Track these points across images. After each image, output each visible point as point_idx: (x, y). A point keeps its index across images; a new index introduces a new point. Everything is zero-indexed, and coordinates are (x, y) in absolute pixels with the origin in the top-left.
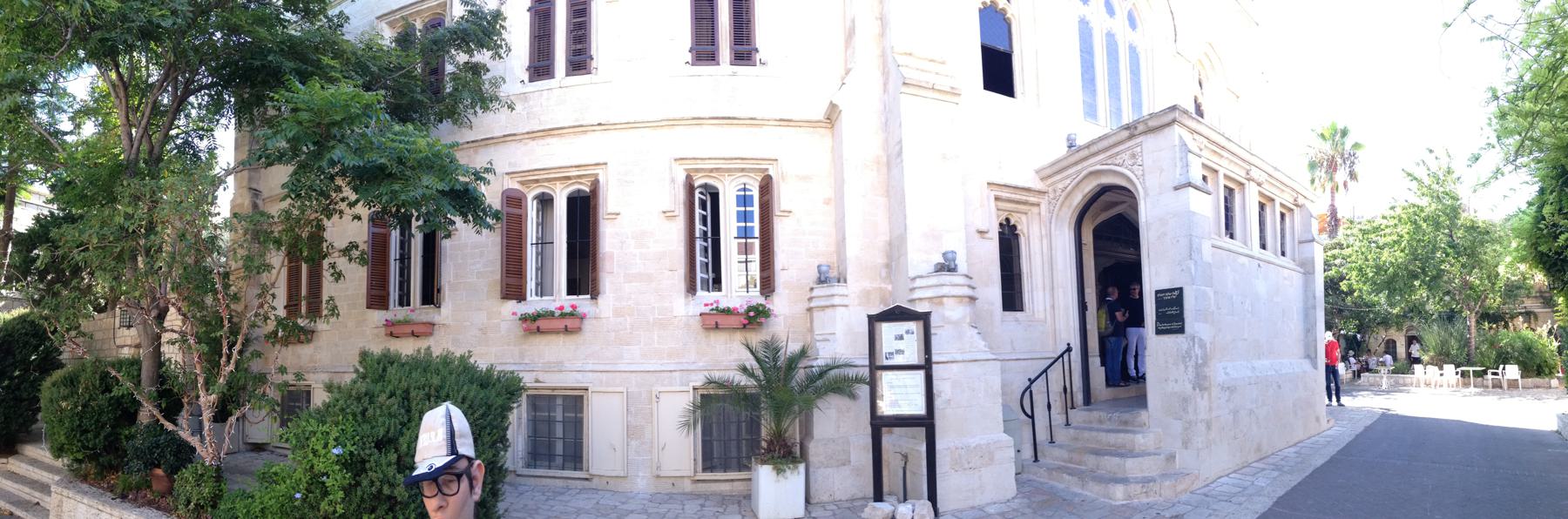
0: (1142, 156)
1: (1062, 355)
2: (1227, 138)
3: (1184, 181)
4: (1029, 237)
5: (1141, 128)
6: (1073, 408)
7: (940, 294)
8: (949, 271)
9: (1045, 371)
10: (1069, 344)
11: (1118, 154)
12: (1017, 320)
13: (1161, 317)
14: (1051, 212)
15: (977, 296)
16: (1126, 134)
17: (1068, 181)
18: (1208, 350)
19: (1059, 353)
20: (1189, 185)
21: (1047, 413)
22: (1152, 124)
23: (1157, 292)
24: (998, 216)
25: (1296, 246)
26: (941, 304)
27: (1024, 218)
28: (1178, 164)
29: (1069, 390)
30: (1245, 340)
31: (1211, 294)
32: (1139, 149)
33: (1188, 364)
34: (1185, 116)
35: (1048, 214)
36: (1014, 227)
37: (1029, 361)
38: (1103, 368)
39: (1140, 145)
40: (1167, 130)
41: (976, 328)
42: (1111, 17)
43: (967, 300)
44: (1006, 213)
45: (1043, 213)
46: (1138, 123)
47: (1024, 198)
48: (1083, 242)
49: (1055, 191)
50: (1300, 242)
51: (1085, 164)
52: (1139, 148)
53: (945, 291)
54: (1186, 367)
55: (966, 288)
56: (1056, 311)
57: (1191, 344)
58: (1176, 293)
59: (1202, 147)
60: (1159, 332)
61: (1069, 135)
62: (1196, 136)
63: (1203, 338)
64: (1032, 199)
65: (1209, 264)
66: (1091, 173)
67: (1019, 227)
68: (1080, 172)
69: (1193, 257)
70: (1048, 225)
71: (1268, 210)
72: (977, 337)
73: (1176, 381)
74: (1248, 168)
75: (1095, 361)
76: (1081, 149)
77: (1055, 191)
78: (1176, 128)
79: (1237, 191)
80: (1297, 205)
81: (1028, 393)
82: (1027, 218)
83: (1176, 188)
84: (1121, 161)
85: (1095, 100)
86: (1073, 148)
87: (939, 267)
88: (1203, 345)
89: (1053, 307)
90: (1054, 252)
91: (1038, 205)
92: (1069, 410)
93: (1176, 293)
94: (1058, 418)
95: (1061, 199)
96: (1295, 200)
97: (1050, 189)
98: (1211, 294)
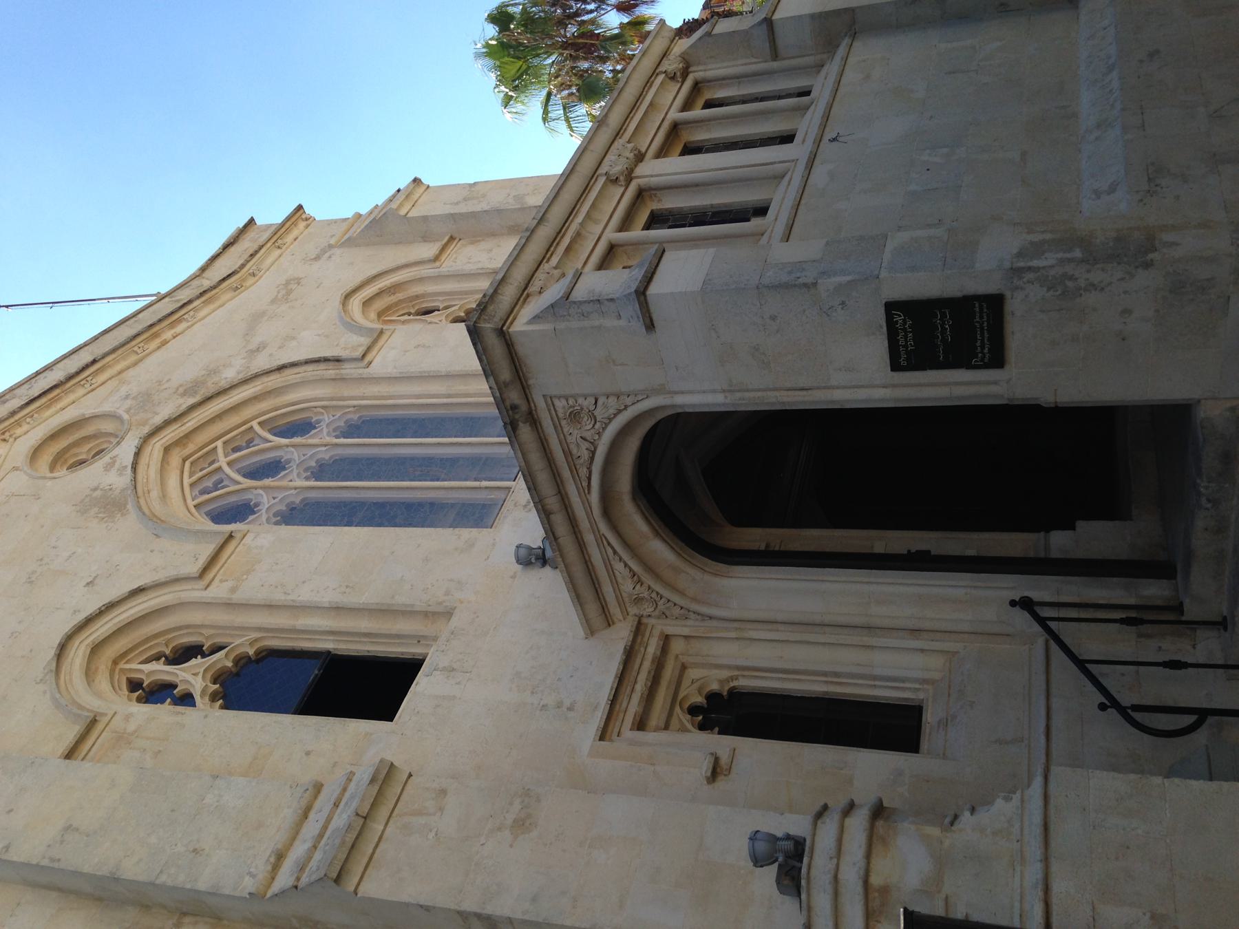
0: (575, 397)
1: (1042, 622)
2: (539, 223)
3: (633, 308)
4: (738, 668)
5: (514, 396)
6: (1179, 608)
7: (859, 889)
8: (799, 857)
9: (1081, 664)
10: (1013, 603)
11: (568, 453)
12: (944, 724)
13: (960, 357)
14: (686, 614)
15: (871, 799)
16: (525, 431)
17: (619, 566)
18: (1048, 236)
19: (1037, 628)
20: (641, 294)
21: (1190, 670)
22: (506, 374)
23: (895, 366)
24: (683, 729)
25: (786, 63)
26: (885, 890)
27: (692, 674)
28: (597, 323)
29: (1133, 614)
30: (1024, 154)
31: (904, 236)
32: (560, 404)
33: (1082, 283)
34: (491, 308)
35: (689, 622)
36: (712, 697)
37: (1056, 703)
38: (1081, 525)
39: (550, 400)
40: (522, 349)
41: (956, 817)
42: (284, 468)
43: (880, 823)
44: (677, 709)
45: (686, 631)
46: (503, 401)
47: (647, 665)
48: (763, 548)
49: (638, 600)
50: (775, 55)
51: (584, 524)
52: (557, 402)
53: (851, 876)
54: (1092, 286)
55: (848, 821)
56: (927, 625)
57: (1031, 276)
58: (899, 319)
59: (557, 273)
60: (997, 360)
61: (519, 561)
62: (533, 288)
63: (1015, 251)
64: (652, 648)
65: (827, 243)
66: (606, 512)
67: (715, 687)
68: (600, 539)
69: (810, 280)
70: (714, 623)
71: (700, 136)
72: (983, 816)
73: (1127, 312)
74: (602, 180)
75: (1060, 542)
76: (551, 534)
77: (638, 600)
78: (520, 325)
79: (655, 205)
80: (685, 73)
81: (1138, 716)
82: (696, 665)
83: (650, 326)
84: (584, 445)
85: (453, 505)
86: (549, 554)
87: (786, 882)
88: (1038, 249)
89: (915, 632)
90: (780, 617)
91: (666, 639)
92: (1184, 618)
93: (899, 319)
94: (1207, 646)
95: (658, 587)
96: (673, 78)
97: (633, 610)
98: (904, 236)
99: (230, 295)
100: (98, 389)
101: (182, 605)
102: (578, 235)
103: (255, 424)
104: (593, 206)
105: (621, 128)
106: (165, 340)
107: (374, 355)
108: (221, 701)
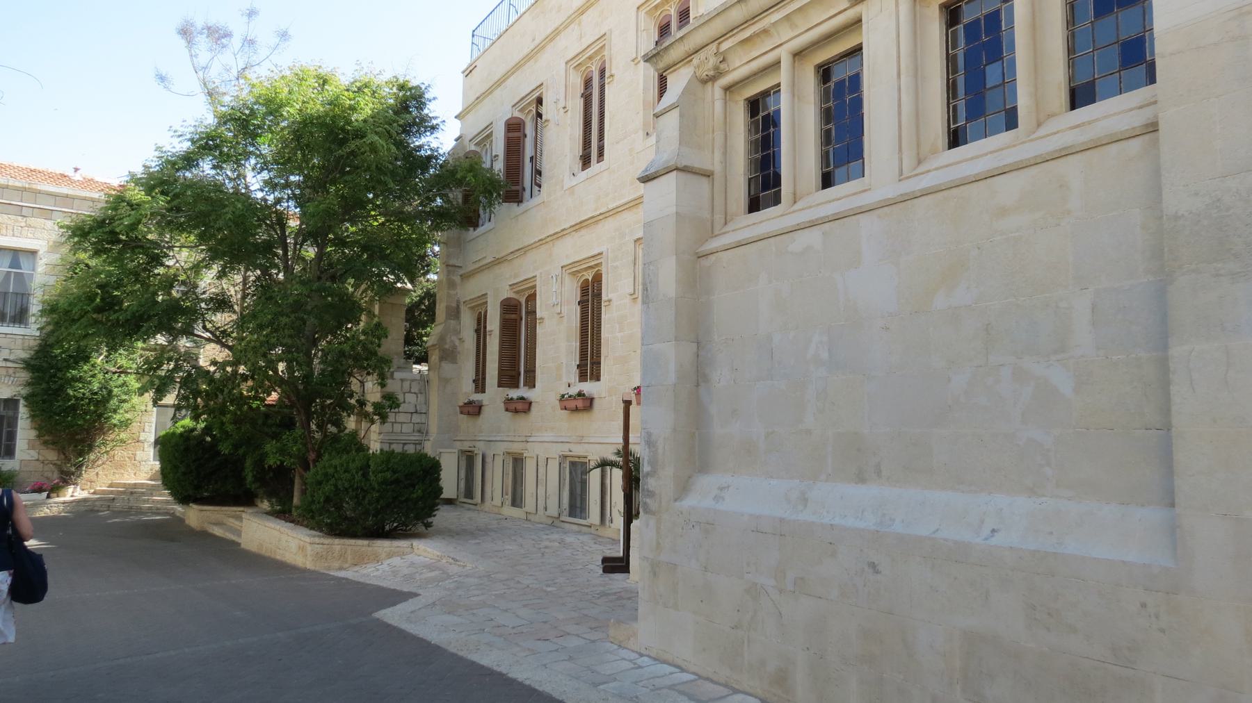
102: (765, 31)
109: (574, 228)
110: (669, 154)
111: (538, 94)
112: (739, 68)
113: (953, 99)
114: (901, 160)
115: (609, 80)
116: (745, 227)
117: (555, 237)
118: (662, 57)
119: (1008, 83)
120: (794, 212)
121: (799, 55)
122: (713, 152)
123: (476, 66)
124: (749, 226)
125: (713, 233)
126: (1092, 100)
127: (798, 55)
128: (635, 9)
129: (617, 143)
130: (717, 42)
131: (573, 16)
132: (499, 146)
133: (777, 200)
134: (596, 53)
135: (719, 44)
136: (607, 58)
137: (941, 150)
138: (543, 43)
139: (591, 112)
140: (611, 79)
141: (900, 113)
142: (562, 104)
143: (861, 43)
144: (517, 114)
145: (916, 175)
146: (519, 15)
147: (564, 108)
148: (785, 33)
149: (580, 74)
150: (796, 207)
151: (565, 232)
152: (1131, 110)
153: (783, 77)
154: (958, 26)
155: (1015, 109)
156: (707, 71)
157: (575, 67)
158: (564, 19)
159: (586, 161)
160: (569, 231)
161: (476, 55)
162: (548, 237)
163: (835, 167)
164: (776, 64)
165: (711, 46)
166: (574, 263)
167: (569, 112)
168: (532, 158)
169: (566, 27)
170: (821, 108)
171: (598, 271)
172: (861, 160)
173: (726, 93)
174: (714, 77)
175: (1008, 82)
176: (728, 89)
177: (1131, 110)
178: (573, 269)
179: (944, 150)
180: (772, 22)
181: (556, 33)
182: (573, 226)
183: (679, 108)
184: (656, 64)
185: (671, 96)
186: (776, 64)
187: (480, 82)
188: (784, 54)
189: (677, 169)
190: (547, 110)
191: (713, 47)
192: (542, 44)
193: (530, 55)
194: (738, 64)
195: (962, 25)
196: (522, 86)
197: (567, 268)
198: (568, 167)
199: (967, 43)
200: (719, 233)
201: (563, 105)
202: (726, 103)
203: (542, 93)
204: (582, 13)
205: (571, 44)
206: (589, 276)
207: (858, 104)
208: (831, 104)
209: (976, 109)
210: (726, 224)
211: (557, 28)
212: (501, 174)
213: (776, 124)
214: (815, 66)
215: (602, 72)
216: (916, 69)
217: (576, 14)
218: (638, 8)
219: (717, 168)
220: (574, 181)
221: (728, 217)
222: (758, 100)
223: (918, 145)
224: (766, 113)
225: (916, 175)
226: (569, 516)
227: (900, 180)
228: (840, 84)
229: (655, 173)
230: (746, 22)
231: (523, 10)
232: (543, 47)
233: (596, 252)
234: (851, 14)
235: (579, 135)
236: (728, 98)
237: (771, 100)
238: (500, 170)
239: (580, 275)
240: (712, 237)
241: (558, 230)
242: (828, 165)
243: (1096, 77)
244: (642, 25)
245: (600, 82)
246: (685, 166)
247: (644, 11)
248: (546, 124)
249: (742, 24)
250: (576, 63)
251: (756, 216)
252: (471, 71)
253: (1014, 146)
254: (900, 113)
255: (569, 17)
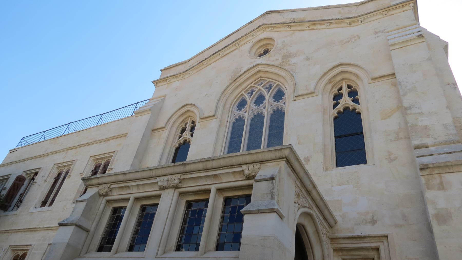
99: (345, 25)
100: (288, 31)
101: (350, 73)
102: (128, 187)
103: (243, 92)
104: (143, 185)
105: (209, 169)
106: (314, 28)
107: (300, 99)
108: (352, 98)
109: (25, 230)
110: (76, 217)
111: (37, 171)
112: (115, 195)
113: (182, 233)
114: (158, 250)
115: (68, 177)
116: (94, 257)
117: (14, 231)
118: (89, 181)
119: (199, 234)
120: (114, 257)
121: (137, 199)
122: (93, 223)
123: (17, 151)
124: (95, 257)
125: (80, 255)
126: (222, 250)
127: (137, 199)
128: (89, 156)
129: (61, 201)
130: (111, 184)
131: (66, 149)
132: (9, 185)
133: (109, 250)
134: (68, 165)
135: (111, 185)
136: (71, 169)
137: (173, 250)
138: (49, 154)
139: (56, 186)
140: (69, 177)
141: (163, 233)
142: (45, 178)
143: (159, 203)
144: (24, 175)
145: (162, 258)
146: (45, 140)
147: (45, 180)
148: (135, 190)
149: (58, 170)
150: (116, 255)
151: (19, 231)
152: (232, 257)
153: (129, 204)
154: (190, 210)
155: (199, 244)
156: (103, 192)
157: (57, 167)
158: (61, 149)
159: (44, 204)
160: (21, 230)
161: (19, 146)
162: (11, 230)
163: (136, 244)
164: (128, 199)
165: (108, 184)
166: (16, 245)
167: (46, 183)
168: (21, 194)
169: (61, 152)
170: (138, 220)
171: (25, 253)
172: (145, 245)
173: (107, 203)
174: (105, 195)
175: (200, 234)
176: (108, 201)
177: (232, 257)
178: (14, 249)
179: (174, 251)
180: (132, 185)
181: (56, 152)
182: (25, 229)
183: (86, 202)
184: (85, 182)
185: (86, 197)
186: (128, 199)
187: (15, 157)
188: (132, 197)
189: (76, 225)
190: (38, 178)
191: (109, 185)
192: (48, 154)
193: (41, 156)
194: (115, 194)
195: (191, 210)
196: (32, 165)
197: (12, 247)
198: (35, 204)
199: (191, 216)
200: (83, 256)
201: (45, 179)
202: (105, 206)
203: (39, 171)
204: (69, 150)
205: (60, 158)
206: (20, 254)
207: (151, 224)
208: (142, 220)
209: (188, 240)
210: (86, 253)
211: (57, 151)
212: (3, 196)
213: (121, 220)
214: (141, 205)
215: (67, 173)
216: (173, 218)
217: (67, 149)
218: (91, 157)
219: (92, 229)
220: (35, 210)
221: (88, 251)
222: (118, 209)
223: (166, 246)
224: (119, 215)
225: (162, 258)
226: (337, 167)
227: (156, 258)
228: (148, 214)
229: (66, 223)
230: (123, 181)
231: (47, 139)
232: (48, 155)
233: (29, 244)
234: (158, 192)
235: (46, 192)
236: (107, 204)
237: (122, 210)
238: (3, 195)
239: (17, 252)
240: (78, 257)
241: (17, 228)
242: (133, 242)
243: (225, 242)
244: (90, 163)
245: (64, 176)
246: (80, 225)
247: (93, 159)
248: (34, 183)
249: (121, 181)
250: (58, 166)
251: (99, 253)
252: (13, 152)
253: (196, 258)
254: (163, 233)
255: (63, 149)
